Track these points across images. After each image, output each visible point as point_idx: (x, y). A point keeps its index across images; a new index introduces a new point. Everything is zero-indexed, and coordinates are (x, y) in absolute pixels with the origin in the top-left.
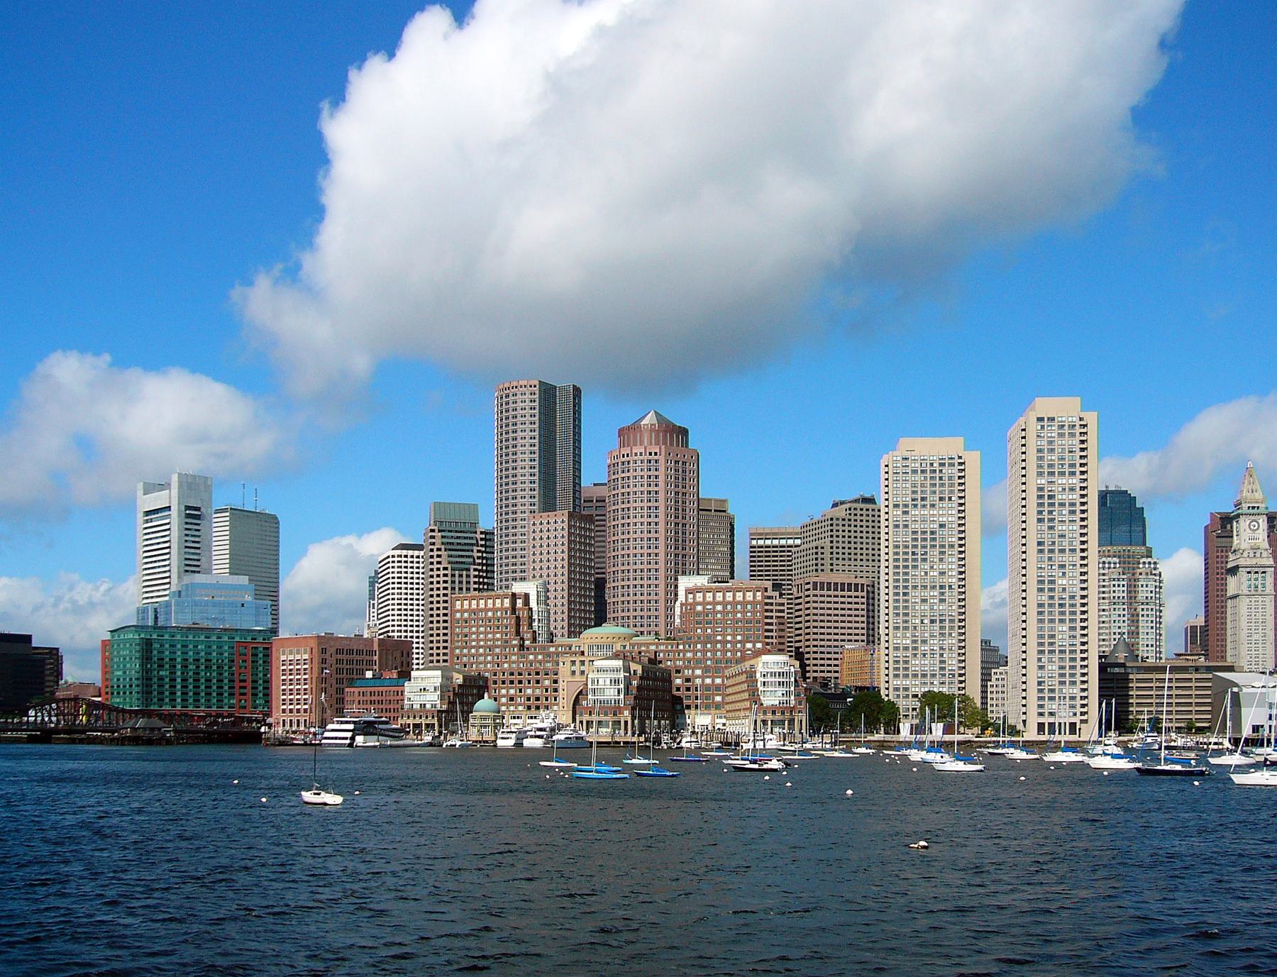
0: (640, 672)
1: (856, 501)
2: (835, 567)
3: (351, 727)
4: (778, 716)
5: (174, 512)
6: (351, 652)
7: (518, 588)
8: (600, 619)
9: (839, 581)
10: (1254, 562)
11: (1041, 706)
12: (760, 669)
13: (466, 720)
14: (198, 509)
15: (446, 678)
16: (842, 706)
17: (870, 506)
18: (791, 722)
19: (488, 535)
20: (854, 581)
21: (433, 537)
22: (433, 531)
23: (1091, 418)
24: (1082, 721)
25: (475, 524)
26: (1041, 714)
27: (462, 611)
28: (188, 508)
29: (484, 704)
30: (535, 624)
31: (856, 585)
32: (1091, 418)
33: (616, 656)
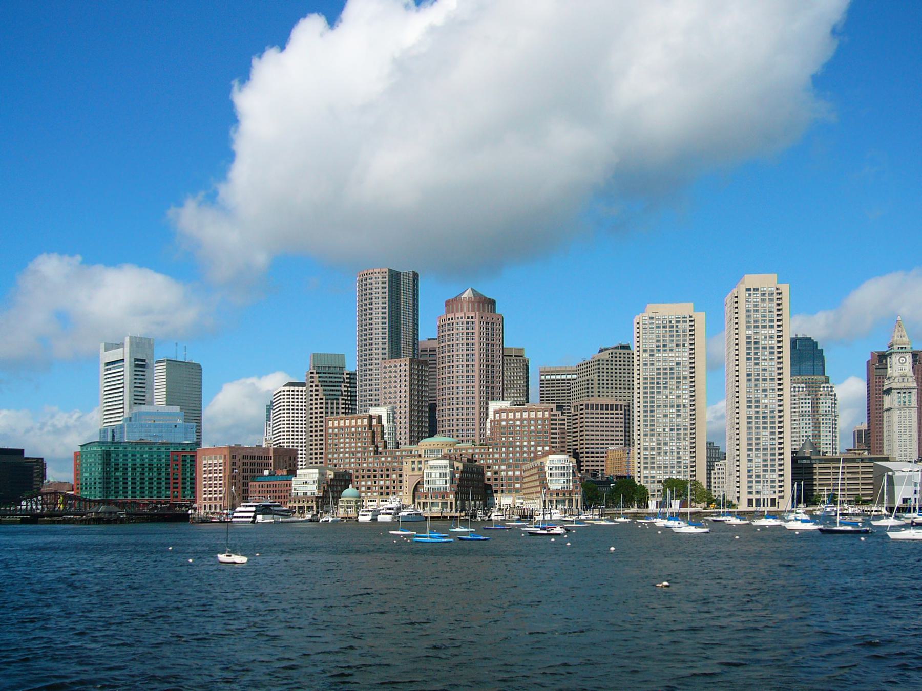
0: (461, 468)
1: (616, 348)
2: (601, 394)
3: (253, 509)
4: (561, 497)
5: (127, 363)
6: (253, 457)
7: (373, 411)
9: (605, 403)
10: (902, 385)
12: (548, 464)
13: (336, 503)
14: (144, 361)
15: (322, 474)
16: (606, 490)
17: (627, 351)
18: (570, 501)
19: (352, 376)
20: (615, 403)
21: (312, 377)
22: (312, 373)
23: (785, 288)
25: (342, 368)
26: (750, 493)
28: (136, 360)
29: (350, 492)
30: (386, 436)
32: (785, 288)
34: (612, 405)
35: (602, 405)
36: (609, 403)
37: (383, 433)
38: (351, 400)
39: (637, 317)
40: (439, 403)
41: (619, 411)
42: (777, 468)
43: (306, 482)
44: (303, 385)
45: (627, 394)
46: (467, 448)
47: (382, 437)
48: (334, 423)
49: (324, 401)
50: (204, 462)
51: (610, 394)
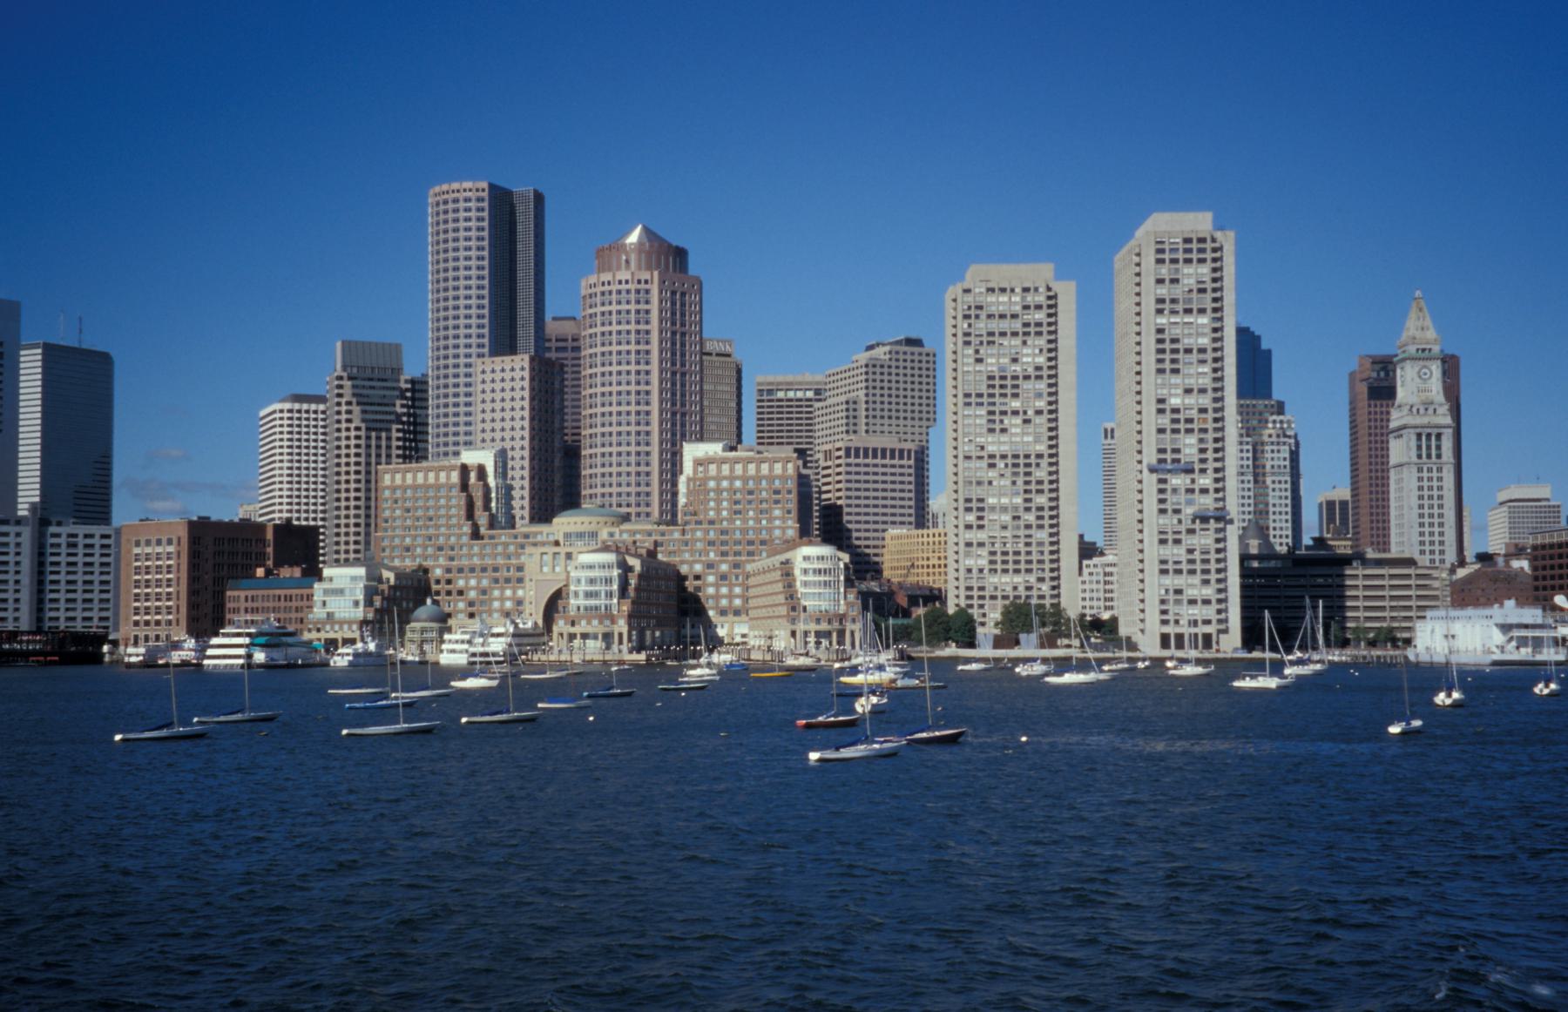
0: (638, 568)
1: (898, 343)
2: (872, 428)
3: (247, 640)
4: (824, 626)
7: (470, 457)
8: (571, 501)
9: (879, 446)
10: (1425, 420)
11: (1164, 612)
12: (799, 565)
13: (402, 633)
15: (374, 577)
16: (896, 610)
17: (916, 350)
18: (841, 633)
19: (418, 388)
20: (898, 446)
21: (340, 387)
22: (341, 378)
23: (1228, 240)
24: (1219, 632)
25: (398, 371)
26: (1165, 622)
27: (394, 489)
30: (493, 504)
31: (902, 451)
32: (1228, 240)
33: (605, 549)
34: (893, 451)
35: (875, 450)
36: (889, 446)
37: (487, 499)
38: (415, 432)
39: (951, 288)
40: (586, 442)
41: (904, 462)
42: (1034, 549)
43: (341, 592)
44: (321, 399)
45: (917, 430)
46: (641, 532)
47: (487, 507)
48: (395, 477)
49: (362, 433)
50: (137, 550)
51: (886, 428)
